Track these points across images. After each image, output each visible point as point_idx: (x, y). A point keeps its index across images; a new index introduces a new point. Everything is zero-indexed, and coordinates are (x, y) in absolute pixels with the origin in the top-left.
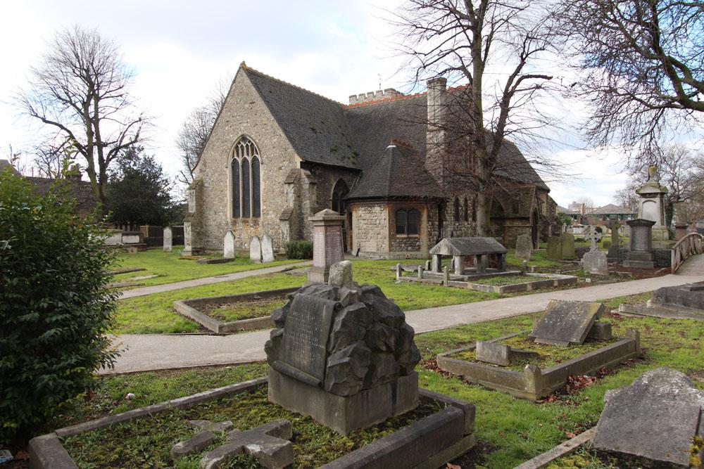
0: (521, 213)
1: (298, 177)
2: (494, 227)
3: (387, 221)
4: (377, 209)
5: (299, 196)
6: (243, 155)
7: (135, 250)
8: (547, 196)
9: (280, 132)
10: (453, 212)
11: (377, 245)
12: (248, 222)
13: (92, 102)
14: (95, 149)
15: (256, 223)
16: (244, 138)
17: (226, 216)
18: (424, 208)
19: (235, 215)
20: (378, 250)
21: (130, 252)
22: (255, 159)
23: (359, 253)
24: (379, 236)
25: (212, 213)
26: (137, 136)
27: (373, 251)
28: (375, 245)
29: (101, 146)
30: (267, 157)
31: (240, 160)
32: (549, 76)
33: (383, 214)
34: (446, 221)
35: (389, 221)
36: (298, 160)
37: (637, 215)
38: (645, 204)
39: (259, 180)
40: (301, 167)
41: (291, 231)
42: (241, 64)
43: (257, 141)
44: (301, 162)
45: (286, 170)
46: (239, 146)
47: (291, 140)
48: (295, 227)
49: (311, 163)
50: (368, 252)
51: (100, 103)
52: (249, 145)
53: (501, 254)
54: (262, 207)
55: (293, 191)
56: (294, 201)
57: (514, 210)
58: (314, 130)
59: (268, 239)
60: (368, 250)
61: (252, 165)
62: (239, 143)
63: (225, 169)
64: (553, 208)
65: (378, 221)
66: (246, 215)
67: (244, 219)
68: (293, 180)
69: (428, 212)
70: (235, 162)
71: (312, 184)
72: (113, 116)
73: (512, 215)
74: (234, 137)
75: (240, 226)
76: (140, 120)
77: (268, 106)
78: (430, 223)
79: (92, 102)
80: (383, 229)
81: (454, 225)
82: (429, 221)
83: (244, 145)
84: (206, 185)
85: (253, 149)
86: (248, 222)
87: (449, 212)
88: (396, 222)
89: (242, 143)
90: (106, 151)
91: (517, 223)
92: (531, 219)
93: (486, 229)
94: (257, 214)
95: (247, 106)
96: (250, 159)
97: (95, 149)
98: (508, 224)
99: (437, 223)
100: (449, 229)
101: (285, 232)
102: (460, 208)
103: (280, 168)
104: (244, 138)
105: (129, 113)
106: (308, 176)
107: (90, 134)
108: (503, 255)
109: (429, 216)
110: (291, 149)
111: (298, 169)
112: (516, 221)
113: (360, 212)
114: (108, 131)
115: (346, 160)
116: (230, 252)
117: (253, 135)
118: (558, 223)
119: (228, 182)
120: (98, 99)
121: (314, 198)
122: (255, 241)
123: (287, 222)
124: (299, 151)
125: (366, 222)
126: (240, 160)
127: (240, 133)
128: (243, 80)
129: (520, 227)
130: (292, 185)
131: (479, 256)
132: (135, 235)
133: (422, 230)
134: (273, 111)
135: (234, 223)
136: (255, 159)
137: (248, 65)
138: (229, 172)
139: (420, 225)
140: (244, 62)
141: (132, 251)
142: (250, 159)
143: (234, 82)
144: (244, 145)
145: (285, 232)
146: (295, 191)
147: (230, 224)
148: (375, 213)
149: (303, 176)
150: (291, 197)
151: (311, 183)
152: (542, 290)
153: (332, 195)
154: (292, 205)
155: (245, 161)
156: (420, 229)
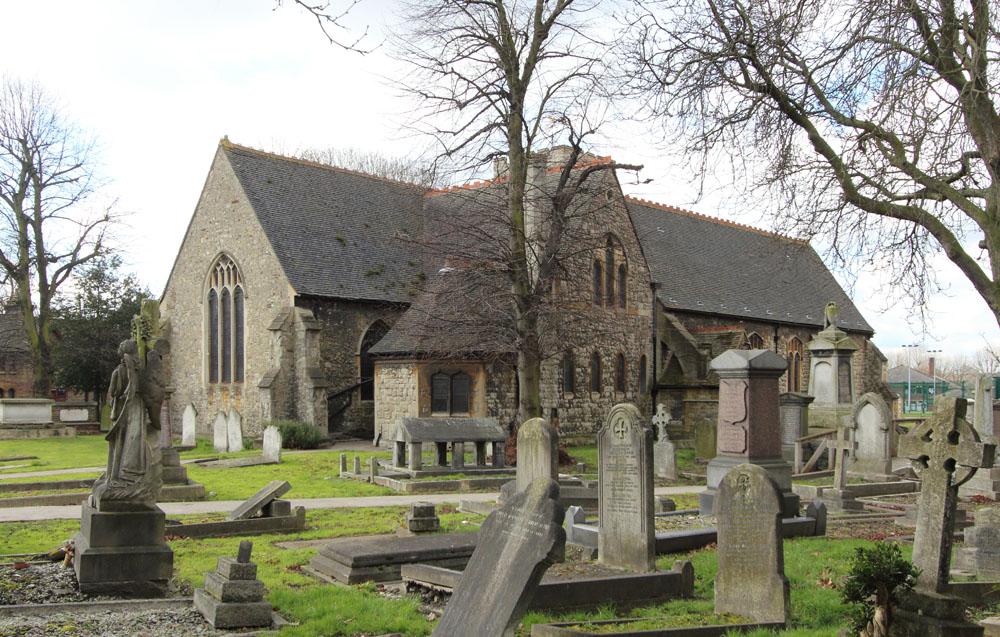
1: (290, 320)
3: (416, 392)
5: (290, 351)
6: (236, 280)
7: (72, 431)
9: (269, 249)
12: (227, 390)
13: (31, 190)
14: (33, 269)
15: (238, 392)
16: (224, 257)
17: (200, 379)
19: (213, 378)
21: (63, 435)
22: (238, 291)
23: (380, 442)
25: (182, 374)
26: (99, 246)
29: (43, 260)
30: (253, 289)
31: (219, 291)
32: (635, 164)
35: (420, 392)
36: (292, 293)
37: (806, 392)
38: (818, 366)
39: (243, 324)
40: (296, 305)
41: (274, 403)
42: (222, 141)
43: (240, 262)
44: (296, 297)
45: (275, 310)
46: (218, 269)
47: (284, 261)
48: (282, 400)
49: (315, 297)
51: (44, 194)
52: (231, 267)
54: (246, 366)
55: (279, 343)
56: (282, 357)
57: (699, 373)
58: (340, 240)
59: (236, 416)
61: (235, 299)
62: (218, 265)
63: (199, 305)
64: (877, 368)
65: (405, 391)
66: (225, 378)
67: (223, 385)
68: (284, 326)
69: (488, 376)
70: (212, 293)
71: (311, 331)
72: (68, 212)
73: (696, 382)
74: (210, 255)
75: (218, 394)
76: (107, 219)
77: (255, 208)
78: (493, 395)
79: (31, 190)
81: (562, 397)
83: (225, 268)
84: (175, 329)
85: (236, 273)
86: (227, 390)
89: (222, 265)
90: (51, 269)
94: (239, 378)
95: (228, 206)
96: (231, 289)
97: (33, 269)
98: (690, 397)
101: (266, 406)
102: (578, 370)
103: (269, 306)
104: (224, 257)
105: (89, 210)
106: (306, 319)
107: (24, 244)
109: (489, 384)
110: (283, 277)
111: (292, 309)
112: (702, 392)
113: (383, 376)
114: (58, 238)
115: (398, 289)
116: (190, 437)
117: (235, 254)
119: (203, 324)
120: (40, 187)
121: (316, 353)
122: (221, 417)
123: (269, 390)
124: (293, 282)
125: (390, 392)
126: (219, 291)
127: (219, 249)
128: (223, 166)
129: (707, 402)
130: (279, 334)
131: (480, 445)
132: (81, 407)
133: (475, 407)
134: (263, 216)
135: (211, 391)
136: (238, 291)
137: (234, 140)
138: (204, 310)
139: (472, 398)
140: (226, 137)
141: (67, 434)
142: (231, 289)
143: (212, 168)
144: (225, 268)
145: (266, 406)
146: (282, 342)
147: (205, 392)
148: (401, 378)
149: (298, 319)
150: (278, 350)
151: (308, 330)
153: (359, 348)
154: (278, 365)
155: (225, 293)
156: (471, 404)
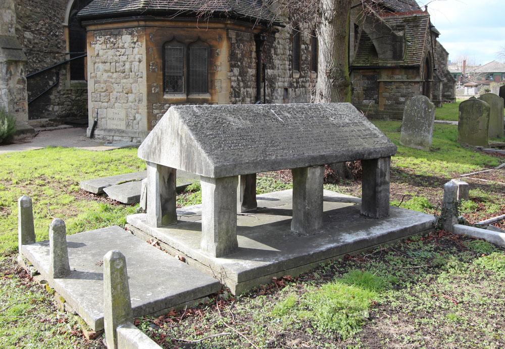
0: (407, 60)
2: (359, 83)
3: (143, 65)
4: (126, 39)
8: (436, 41)
10: (288, 53)
11: (127, 116)
18: (221, 38)
20: (128, 125)
23: (96, 132)
24: (131, 97)
27: (119, 128)
28: (122, 114)
33: (136, 50)
34: (273, 68)
35: (148, 65)
50: (110, 130)
53: (375, 161)
60: (112, 125)
64: (444, 59)
65: (127, 66)
69: (232, 47)
78: (236, 71)
80: (136, 82)
81: (291, 76)
82: (232, 66)
87: (279, 51)
88: (164, 69)
91: (399, 77)
92: (421, 69)
93: (340, 81)
99: (252, 72)
100: (280, 84)
102: (303, 46)
108: (380, 164)
109: (232, 56)
112: (397, 71)
118: (449, 81)
133: (217, 84)
148: (123, 47)
152: (334, 41)
